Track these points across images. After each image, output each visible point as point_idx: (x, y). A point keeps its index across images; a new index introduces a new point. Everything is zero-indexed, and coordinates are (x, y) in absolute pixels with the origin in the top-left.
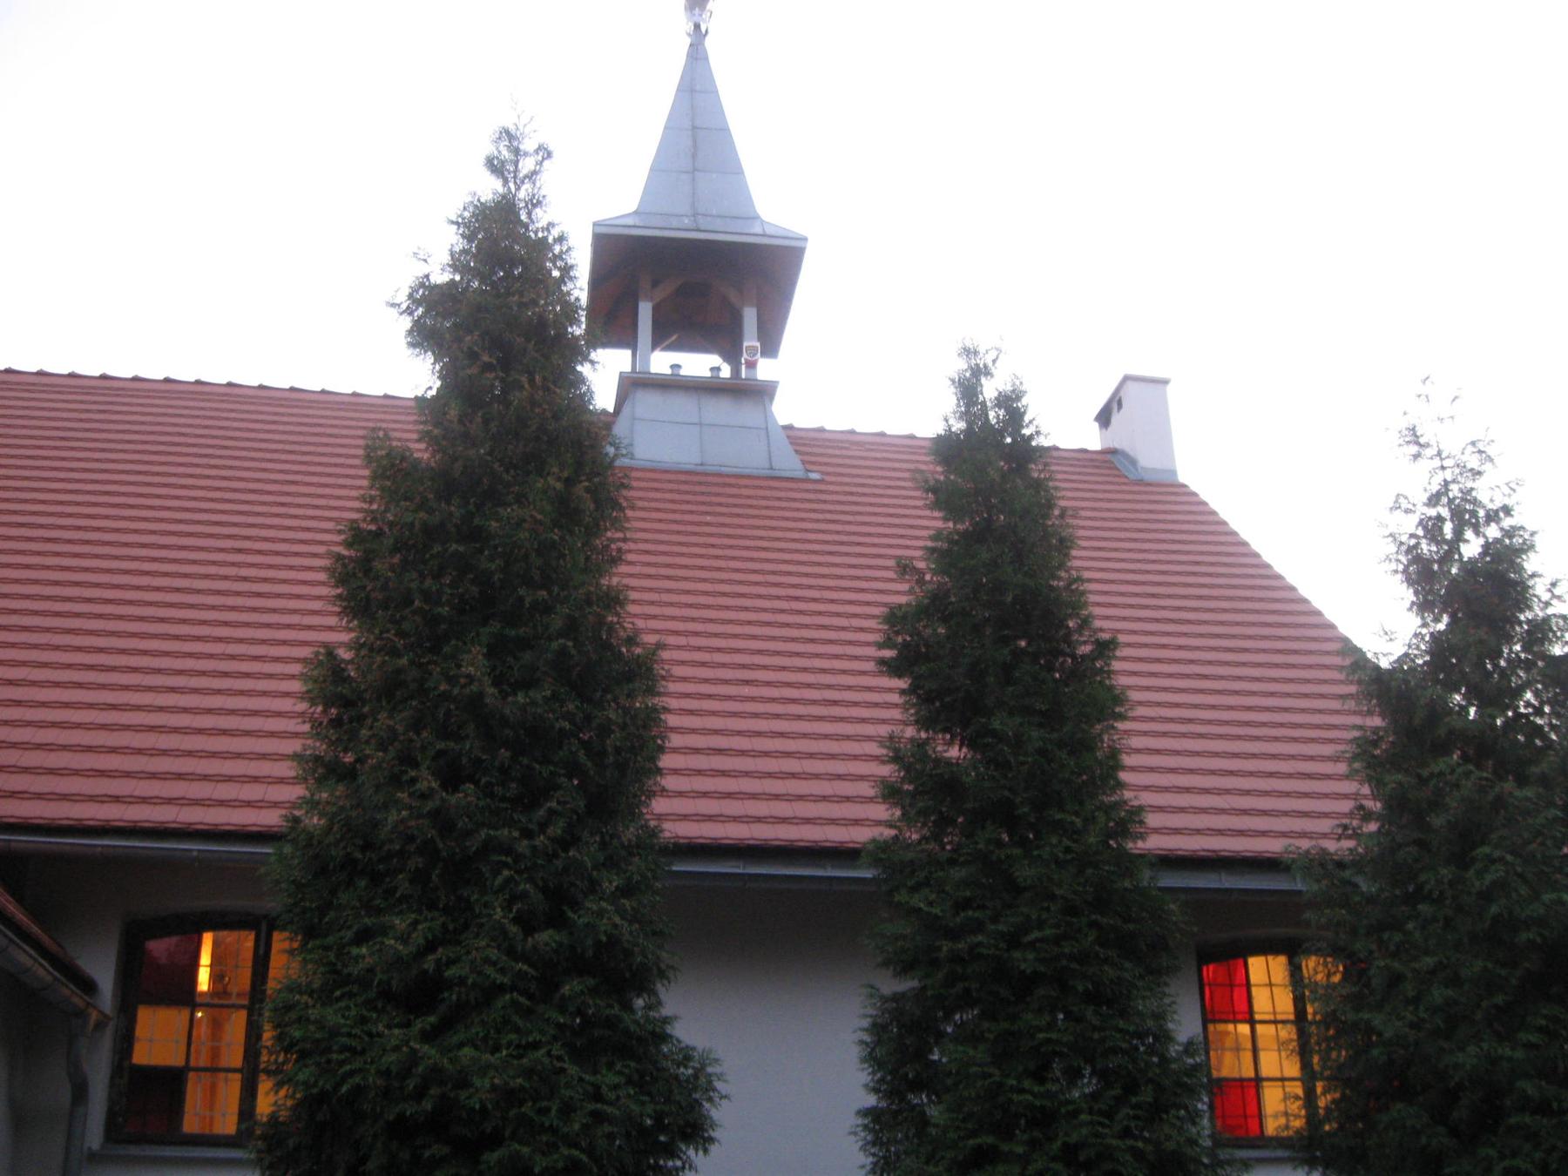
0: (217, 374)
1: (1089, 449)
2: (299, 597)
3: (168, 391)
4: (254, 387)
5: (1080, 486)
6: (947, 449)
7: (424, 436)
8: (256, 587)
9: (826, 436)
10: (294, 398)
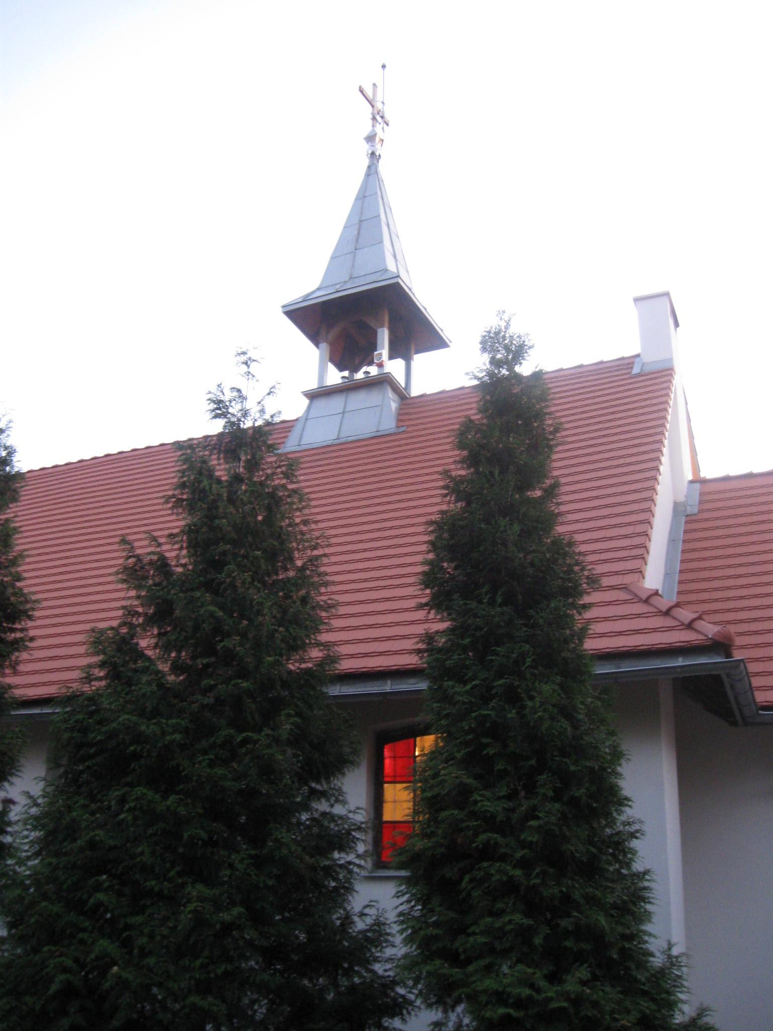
0: (141, 444)
1: (626, 356)
2: (421, 498)
3: (82, 467)
4: (102, 457)
5: (62, 481)
6: (483, 387)
7: (480, 411)
8: (608, 447)
9: (428, 399)
10: (109, 459)
